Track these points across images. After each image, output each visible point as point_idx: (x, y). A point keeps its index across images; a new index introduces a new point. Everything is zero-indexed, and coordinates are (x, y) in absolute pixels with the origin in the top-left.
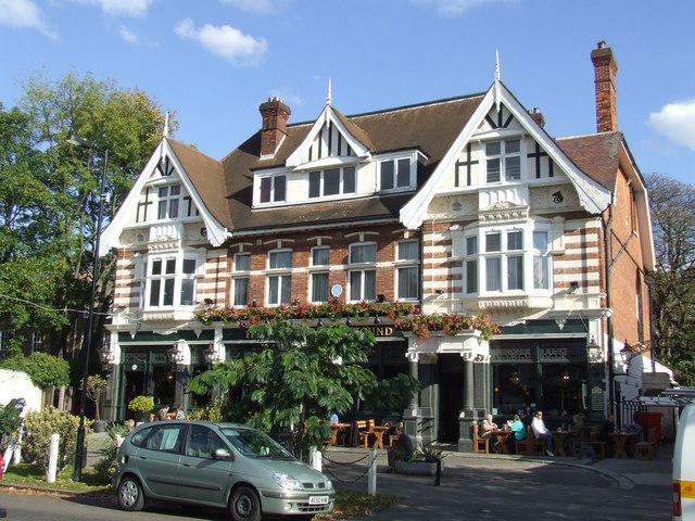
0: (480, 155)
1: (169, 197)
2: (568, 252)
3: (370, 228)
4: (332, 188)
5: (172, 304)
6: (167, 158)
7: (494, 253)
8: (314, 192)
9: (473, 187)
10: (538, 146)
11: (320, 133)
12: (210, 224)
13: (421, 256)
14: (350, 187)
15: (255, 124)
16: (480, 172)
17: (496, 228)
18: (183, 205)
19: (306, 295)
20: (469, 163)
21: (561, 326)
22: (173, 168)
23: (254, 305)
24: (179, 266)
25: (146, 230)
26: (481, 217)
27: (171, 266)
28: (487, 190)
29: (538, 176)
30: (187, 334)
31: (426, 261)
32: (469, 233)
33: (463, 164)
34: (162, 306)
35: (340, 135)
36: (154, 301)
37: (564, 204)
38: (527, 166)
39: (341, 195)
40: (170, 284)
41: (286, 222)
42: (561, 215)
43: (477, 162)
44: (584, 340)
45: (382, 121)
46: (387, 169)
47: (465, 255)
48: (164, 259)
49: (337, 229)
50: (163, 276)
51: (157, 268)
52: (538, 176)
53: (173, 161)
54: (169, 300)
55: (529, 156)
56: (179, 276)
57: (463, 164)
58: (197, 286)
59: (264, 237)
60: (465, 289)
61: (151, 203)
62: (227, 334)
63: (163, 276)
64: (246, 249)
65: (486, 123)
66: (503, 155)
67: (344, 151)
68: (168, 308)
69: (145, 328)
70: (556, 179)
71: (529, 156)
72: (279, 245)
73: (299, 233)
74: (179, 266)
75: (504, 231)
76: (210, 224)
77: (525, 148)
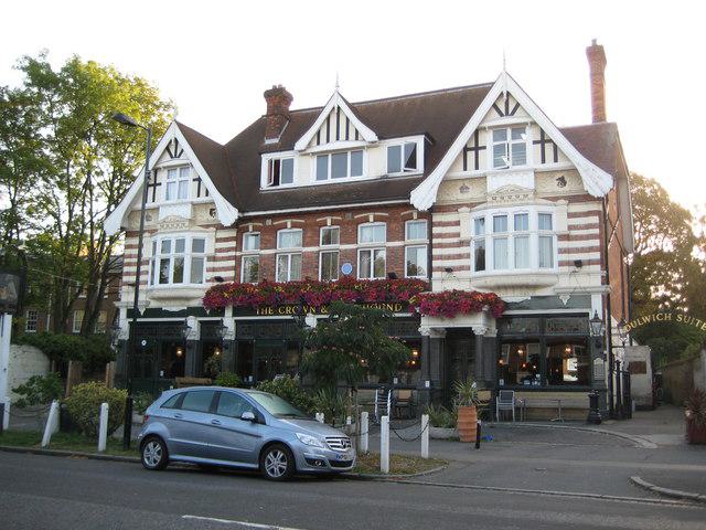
2: (574, 233)
6: (176, 141)
9: (480, 172)
10: (543, 132)
17: (182, 234)
20: (477, 149)
21: (565, 302)
22: (518, 105)
27: (181, 244)
28: (495, 174)
29: (543, 161)
32: (153, 239)
33: (471, 149)
34: (171, 283)
37: (567, 188)
38: (533, 152)
42: (564, 198)
43: (484, 148)
46: (393, 152)
48: (173, 238)
49: (347, 210)
52: (543, 161)
54: (178, 277)
59: (273, 217)
61: (484, 148)
63: (172, 255)
65: (494, 112)
67: (352, 135)
68: (480, 273)
69: (154, 305)
70: (561, 164)
71: (535, 142)
74: (188, 245)
75: (510, 212)
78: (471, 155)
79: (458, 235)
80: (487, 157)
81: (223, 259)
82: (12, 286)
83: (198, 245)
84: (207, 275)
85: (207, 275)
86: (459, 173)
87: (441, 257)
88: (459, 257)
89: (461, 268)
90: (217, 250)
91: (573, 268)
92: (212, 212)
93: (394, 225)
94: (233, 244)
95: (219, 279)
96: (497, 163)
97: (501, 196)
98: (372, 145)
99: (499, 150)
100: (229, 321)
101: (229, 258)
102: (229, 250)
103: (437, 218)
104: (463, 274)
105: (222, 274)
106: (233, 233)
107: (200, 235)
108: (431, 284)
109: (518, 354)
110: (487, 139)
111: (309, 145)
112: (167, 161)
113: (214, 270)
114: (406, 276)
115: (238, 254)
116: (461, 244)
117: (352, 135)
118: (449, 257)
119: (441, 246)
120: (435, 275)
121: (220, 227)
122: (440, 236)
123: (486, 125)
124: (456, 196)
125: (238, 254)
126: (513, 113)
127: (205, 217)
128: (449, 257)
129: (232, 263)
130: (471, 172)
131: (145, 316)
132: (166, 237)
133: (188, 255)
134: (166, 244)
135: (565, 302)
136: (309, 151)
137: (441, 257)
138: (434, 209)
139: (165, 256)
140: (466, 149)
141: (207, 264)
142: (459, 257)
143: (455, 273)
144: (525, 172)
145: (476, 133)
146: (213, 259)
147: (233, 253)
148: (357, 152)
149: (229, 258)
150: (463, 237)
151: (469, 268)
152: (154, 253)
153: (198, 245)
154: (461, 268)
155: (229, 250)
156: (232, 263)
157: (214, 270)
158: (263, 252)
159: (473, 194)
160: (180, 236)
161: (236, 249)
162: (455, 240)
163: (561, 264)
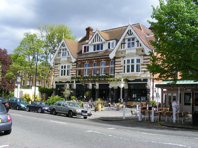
0: (126, 41)
1: (64, 51)
2: (73, 69)
3: (88, 60)
4: (98, 49)
5: (134, 72)
6: (98, 34)
7: (133, 64)
8: (94, 50)
11: (96, 36)
12: (72, 58)
13: (115, 65)
14: (102, 49)
15: (85, 34)
16: (126, 45)
18: (67, 53)
19: (92, 73)
20: (124, 43)
21: (142, 80)
23: (82, 76)
24: (135, 61)
25: (60, 59)
26: (126, 56)
27: (133, 61)
28: (128, 50)
29: (138, 46)
30: (68, 82)
31: (115, 66)
32: (124, 59)
33: (123, 43)
35: (100, 37)
36: (62, 75)
38: (136, 44)
39: (100, 50)
40: (133, 66)
41: (88, 57)
42: (143, 55)
43: (126, 43)
44: (146, 84)
45: (112, 32)
47: (123, 64)
48: (130, 59)
50: (63, 69)
51: (62, 67)
52: (138, 46)
53: (65, 44)
54: (133, 71)
55: (136, 42)
56: (135, 64)
57: (123, 43)
58: (141, 66)
59: (84, 60)
60: (123, 72)
61: (126, 43)
62: (76, 82)
63: (130, 64)
64: (104, 61)
66: (131, 41)
67: (100, 40)
68: (132, 73)
69: (60, 81)
72: (103, 61)
73: (90, 59)
74: (135, 61)
76: (72, 58)
77: (135, 40)
78: (123, 45)
79: (58, 69)
80: (126, 45)
81: (74, 70)
82: (20, 79)
83: (138, 61)
84: (71, 74)
85: (71, 74)
86: (120, 49)
87: (117, 70)
88: (120, 69)
89: (121, 72)
90: (73, 68)
91: (143, 72)
92: (143, 51)
93: (107, 62)
94: (75, 66)
95: (73, 75)
96: (129, 47)
97: (129, 55)
98: (104, 43)
99: (129, 44)
100: (97, 84)
101: (75, 70)
102: (75, 68)
103: (116, 60)
104: (121, 73)
105: (73, 74)
106: (75, 64)
107: (138, 58)
108: (114, 76)
109: (105, 92)
110: (126, 41)
111: (92, 43)
112: (63, 48)
113: (72, 72)
114: (93, 75)
115: (77, 69)
116: (121, 66)
117: (100, 40)
118: (118, 70)
119: (117, 67)
120: (115, 74)
121: (145, 55)
122: (117, 64)
123: (126, 37)
124: (120, 55)
125: (77, 69)
126: (131, 35)
127: (141, 53)
128: (118, 70)
129: (75, 71)
130: (123, 49)
131: (143, 81)
132: (128, 59)
133: (135, 64)
134: (128, 61)
135: (142, 80)
136: (92, 44)
137: (117, 70)
138: (115, 58)
139: (128, 64)
140: (122, 44)
141: (70, 71)
142: (120, 69)
143: (120, 73)
144: (134, 49)
145: (124, 40)
146: (72, 70)
147: (75, 69)
148: (102, 45)
149: (75, 70)
150: (121, 65)
151: (122, 72)
152: (125, 63)
153: (138, 61)
154: (121, 72)
155: (75, 68)
156: (75, 71)
157: (72, 72)
158: (107, 66)
159: (122, 55)
160: (65, 65)
161: (76, 68)
162: (120, 65)
163: (141, 71)
